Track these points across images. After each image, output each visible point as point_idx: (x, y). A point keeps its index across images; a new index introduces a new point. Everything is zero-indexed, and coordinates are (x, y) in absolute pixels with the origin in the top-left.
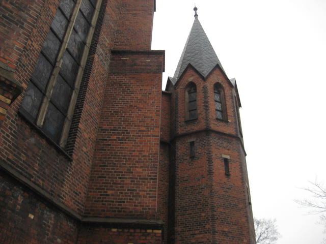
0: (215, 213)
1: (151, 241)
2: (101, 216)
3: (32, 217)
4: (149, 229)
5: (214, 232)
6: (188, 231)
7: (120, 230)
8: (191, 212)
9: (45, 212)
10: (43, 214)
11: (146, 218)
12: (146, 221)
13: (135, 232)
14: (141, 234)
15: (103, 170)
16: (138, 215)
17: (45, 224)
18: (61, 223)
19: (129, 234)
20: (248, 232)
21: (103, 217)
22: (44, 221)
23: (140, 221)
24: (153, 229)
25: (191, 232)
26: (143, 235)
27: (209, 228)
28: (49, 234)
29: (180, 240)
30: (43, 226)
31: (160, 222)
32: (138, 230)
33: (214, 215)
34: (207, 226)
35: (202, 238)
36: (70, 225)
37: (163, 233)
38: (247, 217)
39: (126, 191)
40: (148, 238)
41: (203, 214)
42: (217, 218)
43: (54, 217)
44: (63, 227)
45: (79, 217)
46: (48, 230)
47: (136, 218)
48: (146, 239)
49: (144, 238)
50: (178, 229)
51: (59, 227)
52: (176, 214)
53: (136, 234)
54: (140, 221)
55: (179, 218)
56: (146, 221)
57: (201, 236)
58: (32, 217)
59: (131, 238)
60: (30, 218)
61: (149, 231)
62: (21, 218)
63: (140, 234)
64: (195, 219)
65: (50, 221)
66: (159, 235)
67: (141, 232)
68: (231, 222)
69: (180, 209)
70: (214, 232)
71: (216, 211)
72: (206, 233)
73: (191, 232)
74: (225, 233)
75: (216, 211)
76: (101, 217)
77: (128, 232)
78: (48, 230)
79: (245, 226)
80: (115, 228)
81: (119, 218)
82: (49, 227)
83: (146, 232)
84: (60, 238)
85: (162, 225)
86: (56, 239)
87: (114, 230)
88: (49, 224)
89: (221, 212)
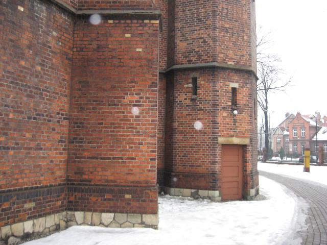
0: (216, 9)
1: (148, 31)
2: (96, 8)
3: (22, 9)
4: (147, 19)
5: (215, 28)
6: (188, 27)
7: (117, 22)
8: (192, 8)
9: (35, 4)
10: (33, 6)
11: (143, 9)
12: (143, 11)
13: (132, 23)
14: (139, 25)
15: (113, 111)
16: (135, 6)
17: (37, 17)
18: (54, 16)
19: (126, 25)
20: (249, 29)
21: (98, 9)
22: (36, 14)
23: (136, 11)
24: (150, 20)
25: (192, 29)
26: (141, 26)
27: (210, 24)
28: (43, 26)
29: (180, 37)
30: (36, 18)
31: (157, 12)
32: (135, 21)
33: (215, 11)
34: (208, 22)
35: (202, 34)
36: (64, 17)
37: (160, 23)
38: (249, 13)
39: (147, 199)
40: (145, 29)
41: (204, 10)
42: (219, 14)
43: (46, 10)
44: (57, 19)
45: (74, 10)
46: (42, 23)
47: (133, 9)
48: (143, 30)
49: (141, 28)
50: (178, 25)
51: (52, 20)
52: (177, 10)
53: (132, 25)
54: (136, 11)
55: (179, 14)
56: (143, 11)
57: (202, 31)
58: (22, 9)
59: (127, 28)
60: (20, 11)
61: (146, 21)
62: (10, 10)
63: (137, 25)
64: (199, 53)
65: (42, 14)
66: (157, 25)
67: (137, 23)
68: (233, 18)
69: (180, 5)
70: (215, 28)
71: (217, 7)
72: (207, 29)
73: (192, 29)
74: (225, 30)
75: (217, 7)
76: (95, 9)
77: (124, 23)
78: (42, 23)
79: (246, 23)
80: (110, 19)
81: (113, 9)
82: (42, 19)
83: (143, 23)
84: (55, 31)
85: (160, 15)
86: (51, 32)
87: (111, 21)
88: (41, 17)
89: (223, 8)
